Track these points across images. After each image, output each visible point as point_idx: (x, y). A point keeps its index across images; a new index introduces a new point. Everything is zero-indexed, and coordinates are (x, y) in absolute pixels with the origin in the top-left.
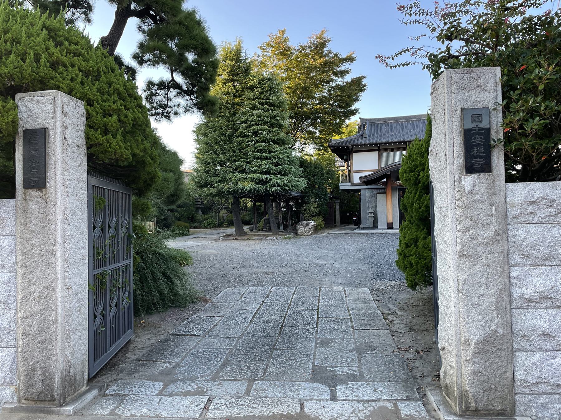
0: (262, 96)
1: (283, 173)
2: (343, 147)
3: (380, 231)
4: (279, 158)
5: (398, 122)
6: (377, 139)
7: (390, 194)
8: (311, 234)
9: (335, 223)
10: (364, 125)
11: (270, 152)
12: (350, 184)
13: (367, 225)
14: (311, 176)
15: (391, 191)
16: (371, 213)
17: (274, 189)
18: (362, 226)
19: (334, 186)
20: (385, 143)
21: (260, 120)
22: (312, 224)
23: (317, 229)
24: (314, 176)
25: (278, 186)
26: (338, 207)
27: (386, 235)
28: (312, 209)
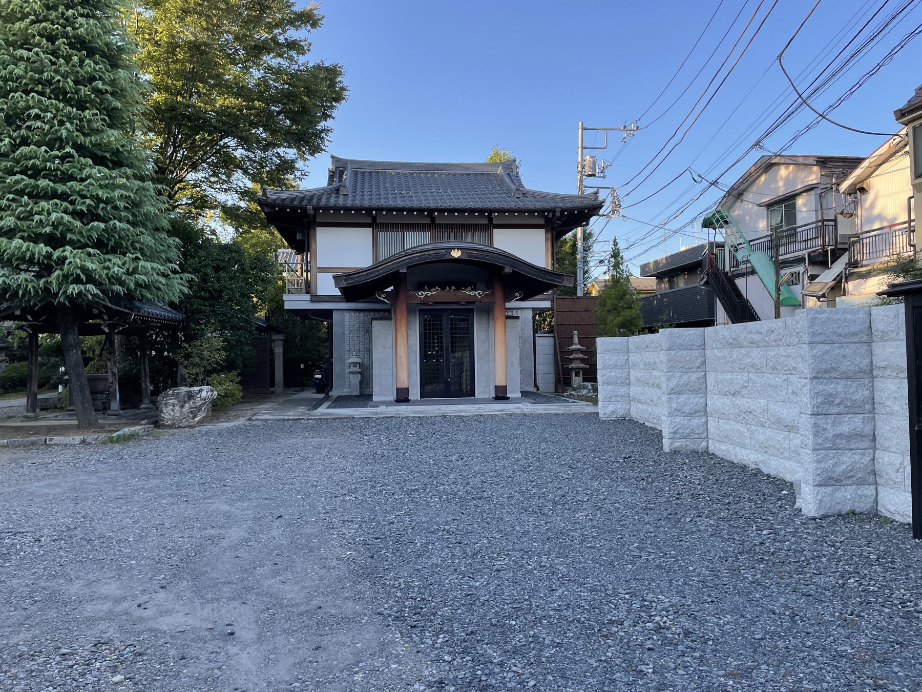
0: (53, 15)
1: (107, 245)
2: (294, 210)
3: (382, 408)
4: (99, 200)
5: (411, 174)
6: (371, 199)
7: (404, 321)
8: (201, 423)
9: (272, 384)
10: (342, 173)
11: (67, 178)
12: (308, 297)
13: (346, 391)
14: (209, 271)
15: (405, 313)
16: (355, 364)
17: (73, 289)
18: (334, 393)
19: (274, 305)
20: (390, 210)
21: (39, 82)
22: (204, 394)
23: (218, 408)
24: (217, 269)
25: (90, 279)
26: (279, 350)
27: (402, 423)
28: (206, 353)
